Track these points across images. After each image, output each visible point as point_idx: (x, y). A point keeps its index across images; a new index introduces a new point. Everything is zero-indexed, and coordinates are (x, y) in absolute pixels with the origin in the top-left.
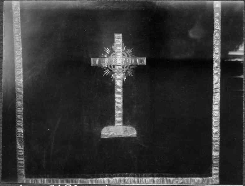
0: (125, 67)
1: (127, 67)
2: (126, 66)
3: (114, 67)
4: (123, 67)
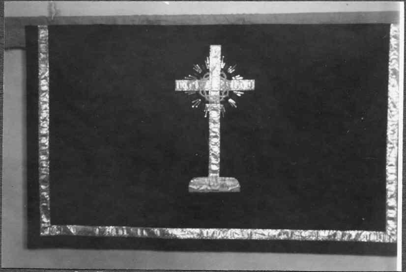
0: (223, 94)
1: (226, 93)
2: (224, 91)
3: (208, 92)
4: (221, 94)
